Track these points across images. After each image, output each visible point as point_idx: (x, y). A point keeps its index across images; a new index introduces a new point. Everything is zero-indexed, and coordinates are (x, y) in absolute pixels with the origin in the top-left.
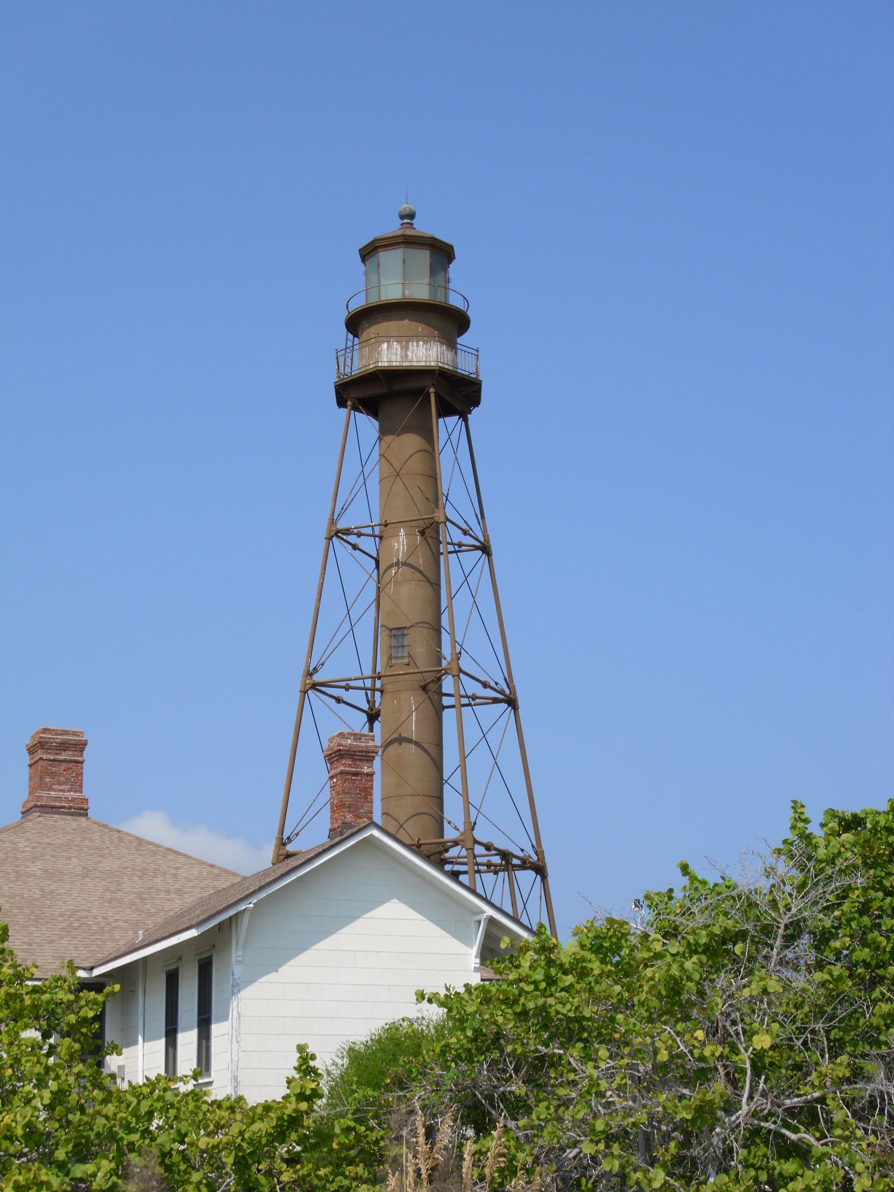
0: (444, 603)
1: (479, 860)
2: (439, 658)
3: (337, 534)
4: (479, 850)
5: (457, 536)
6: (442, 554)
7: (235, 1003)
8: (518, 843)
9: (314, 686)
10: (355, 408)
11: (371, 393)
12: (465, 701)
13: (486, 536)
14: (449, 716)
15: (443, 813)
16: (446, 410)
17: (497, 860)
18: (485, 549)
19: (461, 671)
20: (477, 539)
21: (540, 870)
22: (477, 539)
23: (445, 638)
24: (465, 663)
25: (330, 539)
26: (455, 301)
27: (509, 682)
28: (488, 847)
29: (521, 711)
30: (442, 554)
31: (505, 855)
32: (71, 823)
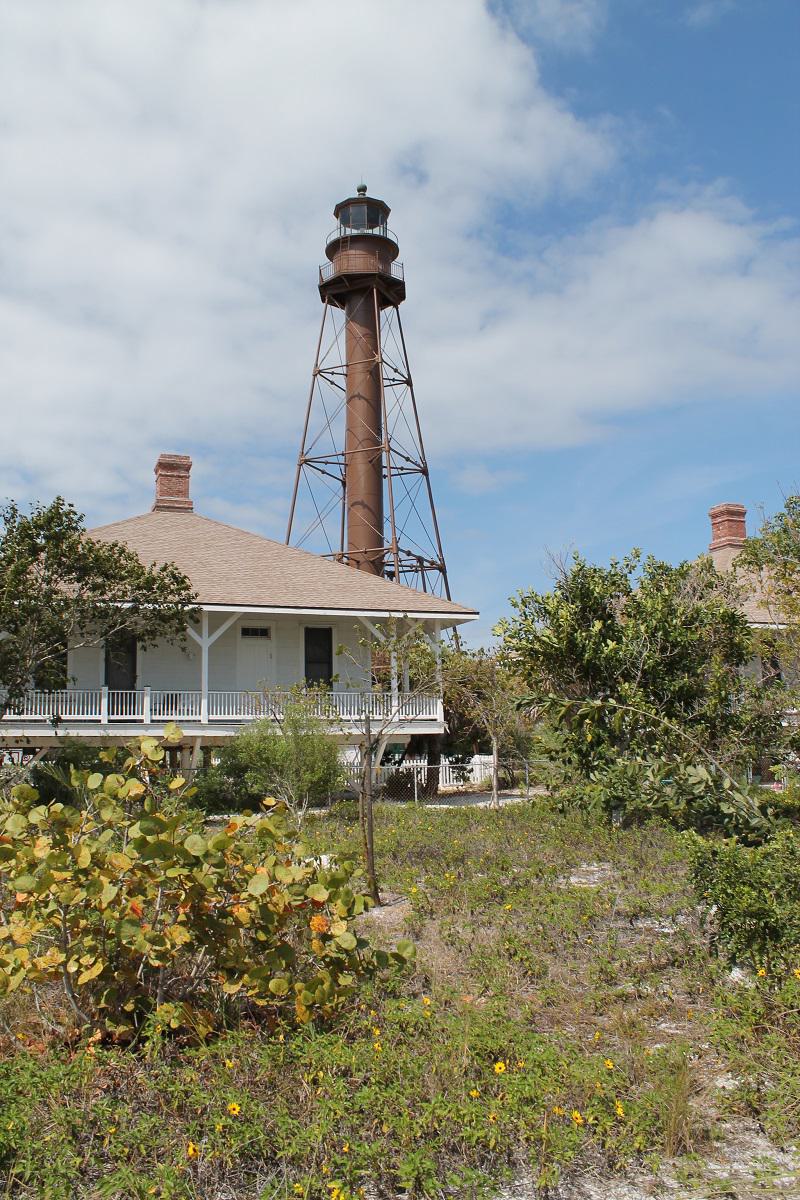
0: (386, 512)
1: (403, 563)
2: (380, 541)
3: (318, 372)
4: (402, 555)
5: (400, 462)
6: (385, 477)
7: (358, 252)
8: (430, 554)
9: (306, 461)
10: (331, 303)
11: (336, 291)
12: (394, 472)
13: (409, 375)
14: (385, 482)
15: (382, 533)
16: (385, 303)
17: (415, 563)
18: (409, 382)
19: (390, 448)
20: (419, 466)
21: (442, 569)
22: (419, 466)
23: (387, 526)
24: (393, 445)
25: (315, 375)
26: (390, 236)
27: (423, 458)
28: (409, 553)
29: (448, 574)
30: (385, 477)
31: (420, 560)
32: (185, 515)
